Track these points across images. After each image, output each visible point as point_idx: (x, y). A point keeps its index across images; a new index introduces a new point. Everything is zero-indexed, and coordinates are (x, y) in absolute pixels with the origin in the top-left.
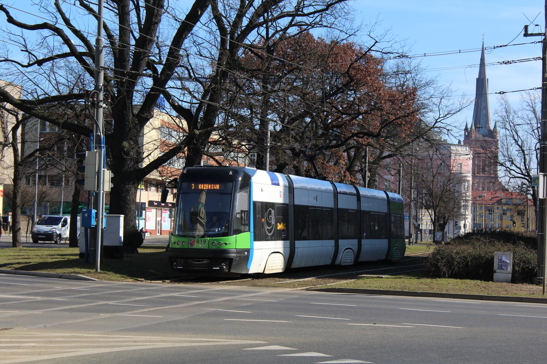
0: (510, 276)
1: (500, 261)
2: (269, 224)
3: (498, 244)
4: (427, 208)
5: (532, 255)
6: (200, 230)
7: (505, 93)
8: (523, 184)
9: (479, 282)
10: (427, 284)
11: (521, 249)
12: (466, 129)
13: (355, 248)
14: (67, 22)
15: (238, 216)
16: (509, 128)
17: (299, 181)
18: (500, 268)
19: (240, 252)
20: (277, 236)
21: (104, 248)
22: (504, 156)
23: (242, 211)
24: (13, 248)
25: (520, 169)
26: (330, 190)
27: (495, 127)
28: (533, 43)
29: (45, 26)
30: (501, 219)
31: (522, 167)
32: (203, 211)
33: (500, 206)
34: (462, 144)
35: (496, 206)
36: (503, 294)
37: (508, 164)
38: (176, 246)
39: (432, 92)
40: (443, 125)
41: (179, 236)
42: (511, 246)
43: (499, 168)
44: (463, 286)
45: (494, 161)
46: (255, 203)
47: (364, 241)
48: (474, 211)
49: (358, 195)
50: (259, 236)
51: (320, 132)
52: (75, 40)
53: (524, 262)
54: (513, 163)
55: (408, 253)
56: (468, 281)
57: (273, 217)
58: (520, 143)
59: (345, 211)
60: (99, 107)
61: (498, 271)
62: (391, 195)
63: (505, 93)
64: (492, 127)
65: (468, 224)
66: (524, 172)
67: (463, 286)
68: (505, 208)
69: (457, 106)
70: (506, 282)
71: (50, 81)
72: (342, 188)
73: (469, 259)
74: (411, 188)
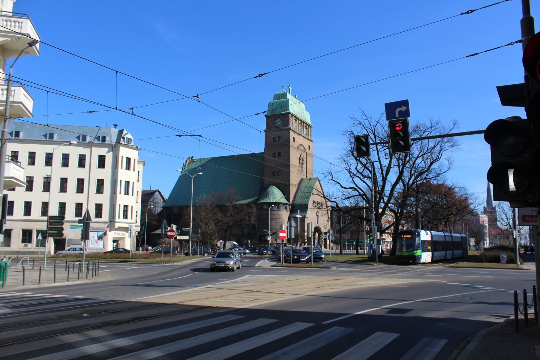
0: (506, 261)
1: (503, 257)
2: (426, 247)
3: (501, 251)
4: (473, 237)
5: (513, 255)
6: (404, 250)
7: (474, 11)
8: (507, 228)
9: (496, 264)
10: (479, 265)
11: (510, 253)
12: (484, 207)
13: (452, 253)
14: (356, 185)
15: (417, 245)
16: (501, 208)
17: (434, 233)
18: (503, 259)
19: (418, 256)
20: (428, 251)
21: (170, 253)
22: (500, 218)
23: (418, 244)
24: (340, 256)
25: (506, 222)
26: (443, 235)
27: (495, 206)
28: (508, 45)
29: (352, 188)
30: (500, 240)
31: (507, 222)
32: (404, 243)
33: (499, 235)
34: (483, 213)
35: (497, 235)
36: (504, 267)
37: (501, 221)
38: (398, 255)
39: (472, 197)
40: (477, 209)
41: (399, 251)
42: (506, 252)
43: (498, 222)
44: (491, 265)
45: (496, 220)
46: (422, 241)
47: (454, 251)
48: (489, 238)
49: (452, 236)
50: (423, 251)
51: (435, 214)
52: (360, 191)
53: (510, 257)
54: (503, 221)
55: (469, 254)
56: (492, 263)
57: (427, 245)
58: (505, 213)
59: (448, 241)
60: (373, 213)
61: (502, 260)
62: (462, 235)
63: (474, 11)
64: (494, 206)
65: (487, 242)
66: (507, 223)
67: (491, 265)
68: (501, 236)
69: (482, 202)
70: (505, 263)
71: (348, 202)
72: (447, 234)
73: (492, 256)
74: (467, 231)
